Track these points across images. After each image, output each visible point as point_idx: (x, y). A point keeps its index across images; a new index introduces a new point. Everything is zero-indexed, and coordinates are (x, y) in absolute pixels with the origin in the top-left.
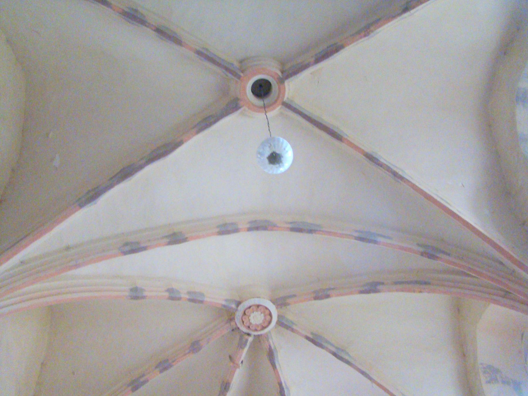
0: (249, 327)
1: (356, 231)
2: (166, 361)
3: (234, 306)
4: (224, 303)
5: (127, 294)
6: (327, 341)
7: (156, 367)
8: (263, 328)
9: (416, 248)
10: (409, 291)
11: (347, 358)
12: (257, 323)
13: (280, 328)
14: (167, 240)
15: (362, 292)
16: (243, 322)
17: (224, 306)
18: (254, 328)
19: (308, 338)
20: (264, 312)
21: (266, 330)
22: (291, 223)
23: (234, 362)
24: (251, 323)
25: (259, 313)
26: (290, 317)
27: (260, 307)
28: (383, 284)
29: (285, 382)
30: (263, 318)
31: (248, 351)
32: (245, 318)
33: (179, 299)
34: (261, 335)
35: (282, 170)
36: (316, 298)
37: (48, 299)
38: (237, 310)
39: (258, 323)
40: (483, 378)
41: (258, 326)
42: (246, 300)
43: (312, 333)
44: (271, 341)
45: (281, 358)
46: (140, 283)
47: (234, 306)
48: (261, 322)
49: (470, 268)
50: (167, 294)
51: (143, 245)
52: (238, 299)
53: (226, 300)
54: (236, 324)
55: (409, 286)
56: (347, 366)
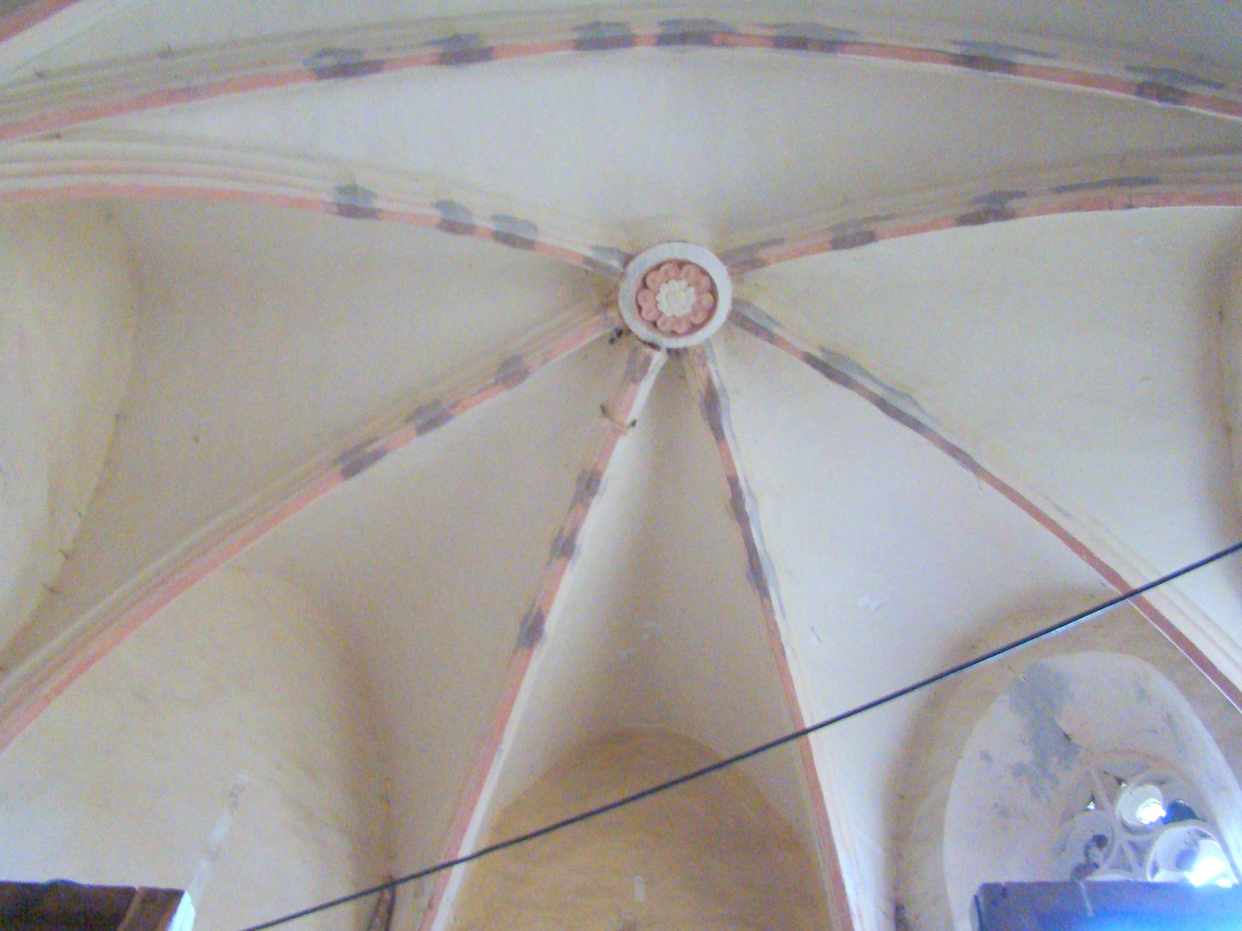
0: (654, 324)
1: (955, 42)
3: (615, 263)
4: (590, 254)
6: (865, 374)
8: (694, 328)
11: (911, 411)
13: (738, 331)
15: (964, 220)
16: (640, 308)
17: (589, 261)
18: (667, 327)
19: (810, 359)
20: (696, 284)
22: (775, 27)
24: (660, 314)
25: (684, 283)
26: (763, 304)
27: (685, 269)
28: (1023, 194)
30: (693, 299)
32: (646, 300)
34: (685, 350)
36: (839, 243)
37: (113, 180)
38: (623, 275)
39: (679, 313)
41: (677, 321)
43: (823, 349)
44: (711, 366)
45: (736, 415)
47: (615, 263)
48: (687, 310)
50: (437, 214)
52: (626, 249)
53: (597, 248)
54: (620, 316)
55: (1095, 194)
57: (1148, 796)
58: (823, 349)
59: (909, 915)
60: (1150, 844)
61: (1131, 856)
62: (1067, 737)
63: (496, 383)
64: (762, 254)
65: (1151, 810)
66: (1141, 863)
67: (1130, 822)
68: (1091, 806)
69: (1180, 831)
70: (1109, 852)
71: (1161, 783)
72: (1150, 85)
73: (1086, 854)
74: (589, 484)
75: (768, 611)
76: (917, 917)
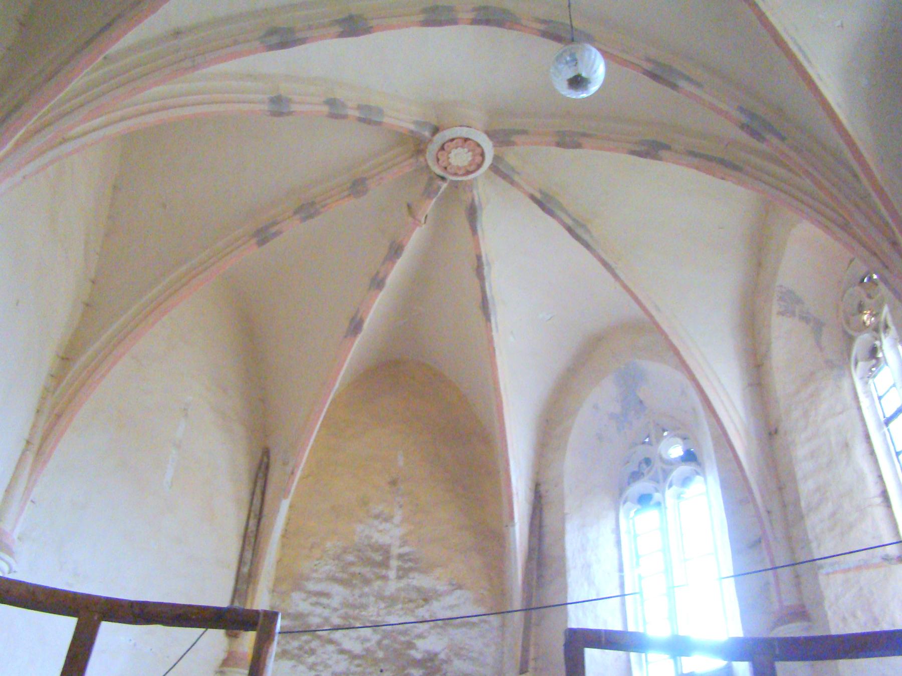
0: (446, 168)
2: (313, 204)
3: (427, 134)
4: (412, 127)
5: (265, 107)
6: (563, 210)
7: (295, 213)
8: (468, 173)
9: (735, 114)
10: (708, 172)
11: (586, 237)
12: (460, 165)
14: (337, 29)
15: (633, 153)
16: (438, 160)
17: (412, 132)
18: (453, 171)
19: (532, 198)
21: (471, 177)
23: (414, 217)
24: (450, 164)
25: (466, 150)
27: (468, 142)
29: (486, 255)
31: (435, 202)
33: (344, 117)
35: (593, 88)
38: (430, 141)
40: (775, 307)
41: (459, 168)
42: (448, 128)
43: (541, 192)
44: (475, 192)
45: (485, 220)
46: (285, 89)
48: (466, 163)
49: (807, 171)
50: (325, 109)
51: (299, 35)
53: (416, 123)
54: (426, 160)
56: (584, 250)
57: (677, 443)
58: (541, 192)
59: (542, 489)
60: (671, 471)
61: (661, 477)
62: (641, 402)
63: (350, 195)
64: (514, 138)
65: (676, 451)
66: (665, 479)
67: (664, 456)
68: (647, 440)
69: (686, 468)
70: (651, 469)
71: (684, 438)
72: (748, 127)
73: (639, 466)
74: (396, 250)
75: (489, 330)
76: (547, 492)
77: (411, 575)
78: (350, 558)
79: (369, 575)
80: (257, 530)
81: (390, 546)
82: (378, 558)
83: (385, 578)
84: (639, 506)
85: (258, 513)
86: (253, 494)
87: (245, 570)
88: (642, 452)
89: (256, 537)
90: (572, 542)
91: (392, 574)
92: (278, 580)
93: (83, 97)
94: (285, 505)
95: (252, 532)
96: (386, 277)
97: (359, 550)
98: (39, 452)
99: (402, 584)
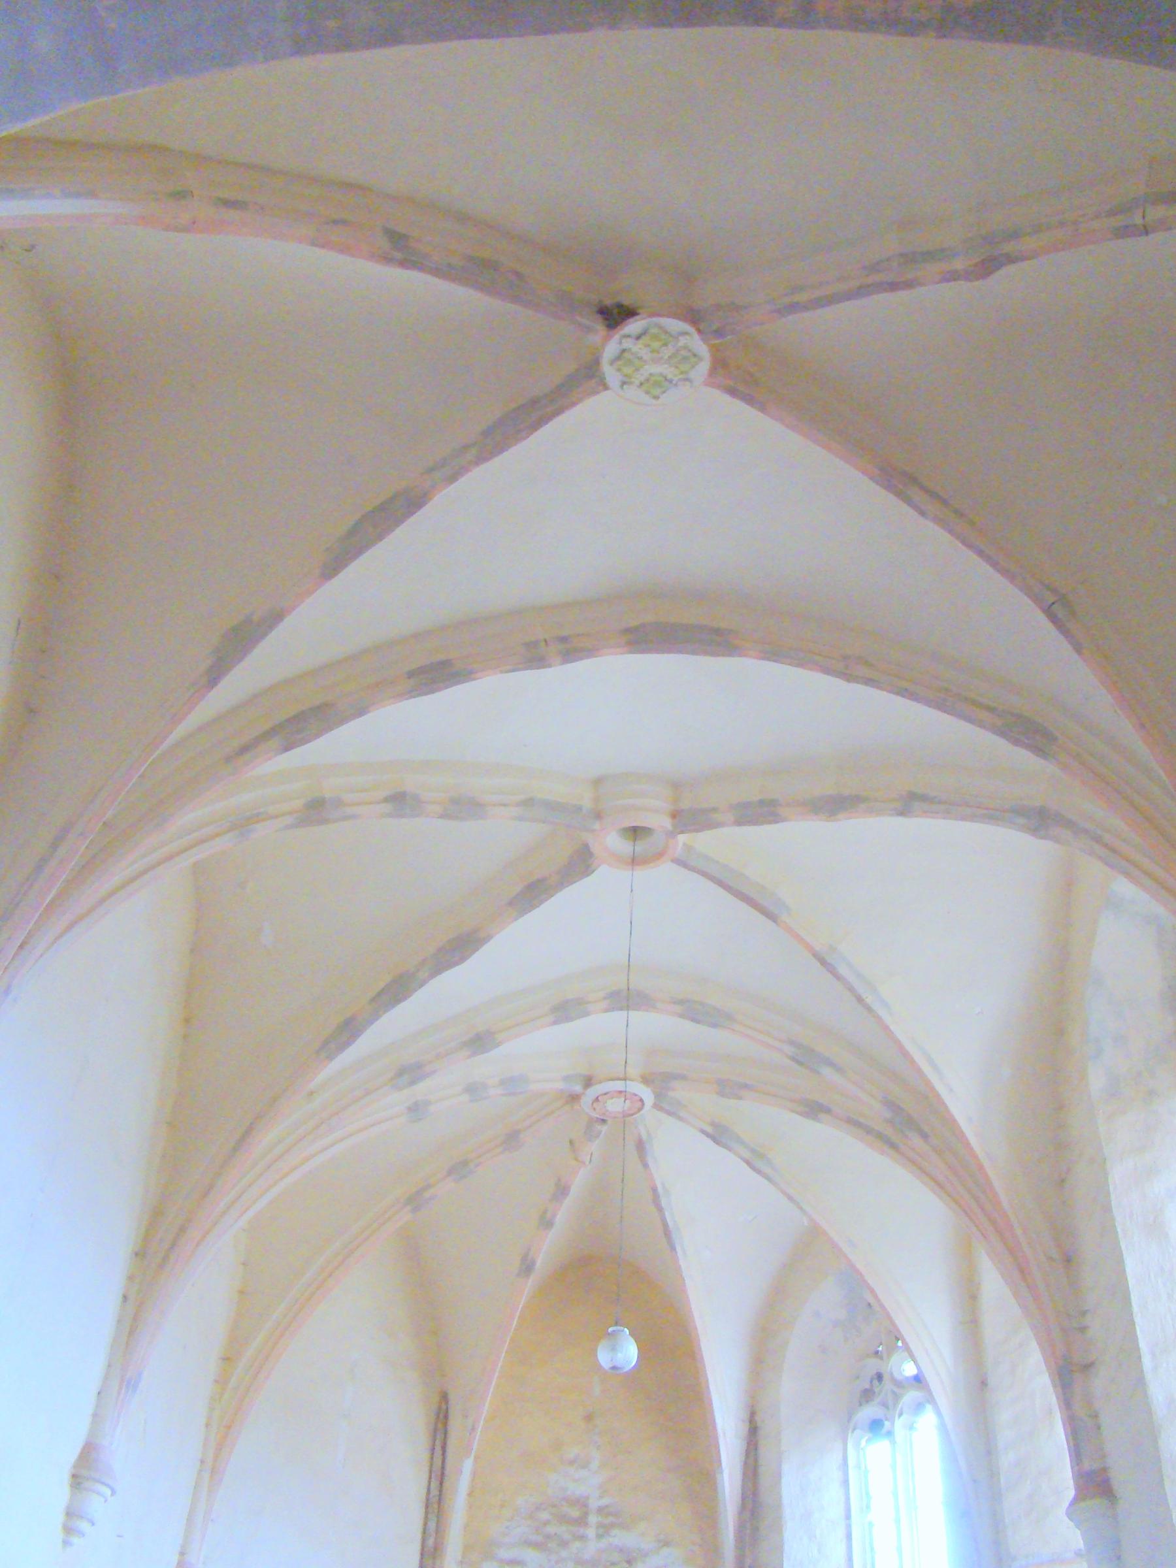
4: (560, 1085)
24: (607, 1111)
53: (566, 1079)
59: (757, 1418)
66: (895, 1405)
67: (896, 1375)
73: (871, 1382)
77: (615, 1532)
78: (544, 1516)
79: (567, 1536)
80: (440, 1495)
81: (587, 1498)
82: (575, 1513)
83: (582, 1538)
84: (870, 1435)
85: (439, 1473)
86: (433, 1450)
87: (430, 1542)
88: (872, 1365)
89: (440, 1501)
90: (789, 1487)
91: (591, 1532)
92: (467, 1548)
93: (195, 835)
94: (468, 1465)
95: (434, 1497)
96: (554, 1215)
97: (554, 1506)
98: (213, 1471)
99: (603, 1543)
